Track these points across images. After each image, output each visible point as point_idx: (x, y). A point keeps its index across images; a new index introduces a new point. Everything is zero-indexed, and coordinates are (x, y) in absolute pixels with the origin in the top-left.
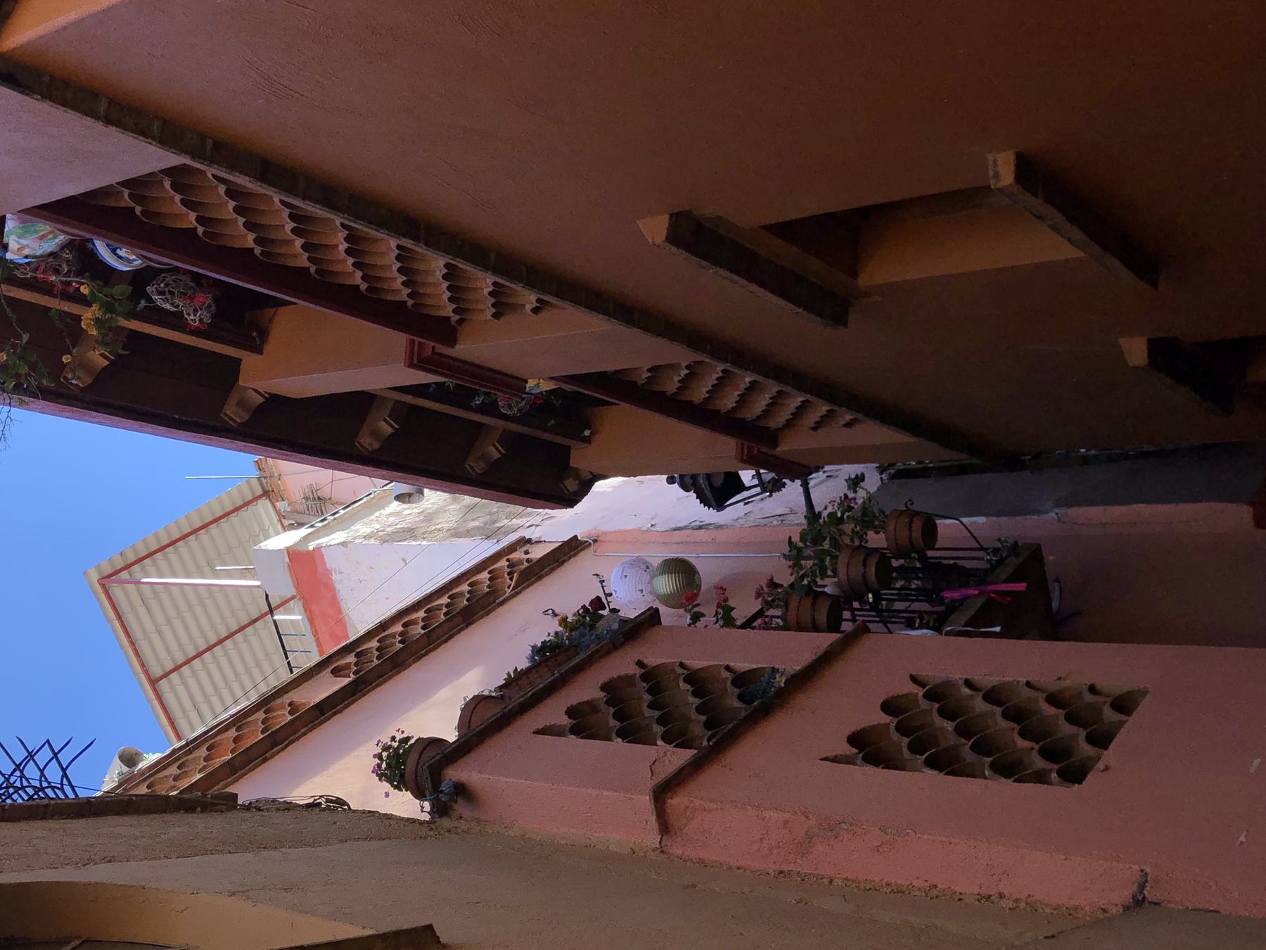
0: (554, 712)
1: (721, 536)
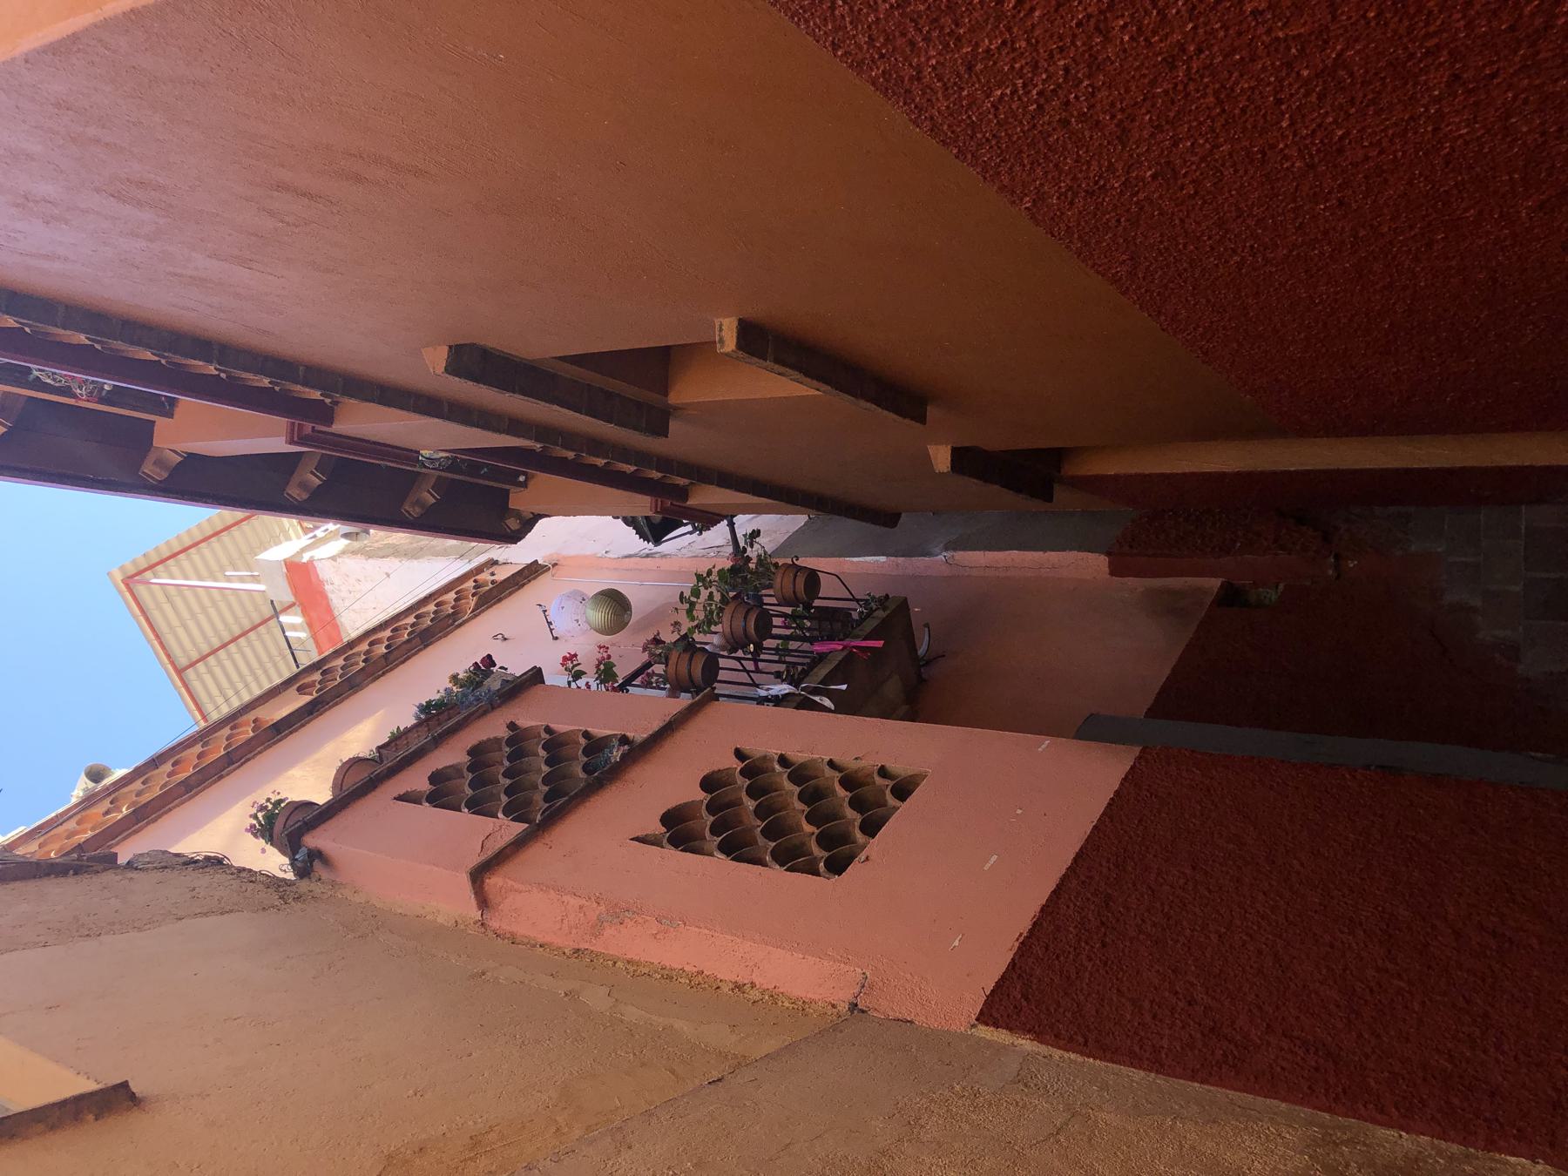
0: (417, 779)
1: (665, 565)
